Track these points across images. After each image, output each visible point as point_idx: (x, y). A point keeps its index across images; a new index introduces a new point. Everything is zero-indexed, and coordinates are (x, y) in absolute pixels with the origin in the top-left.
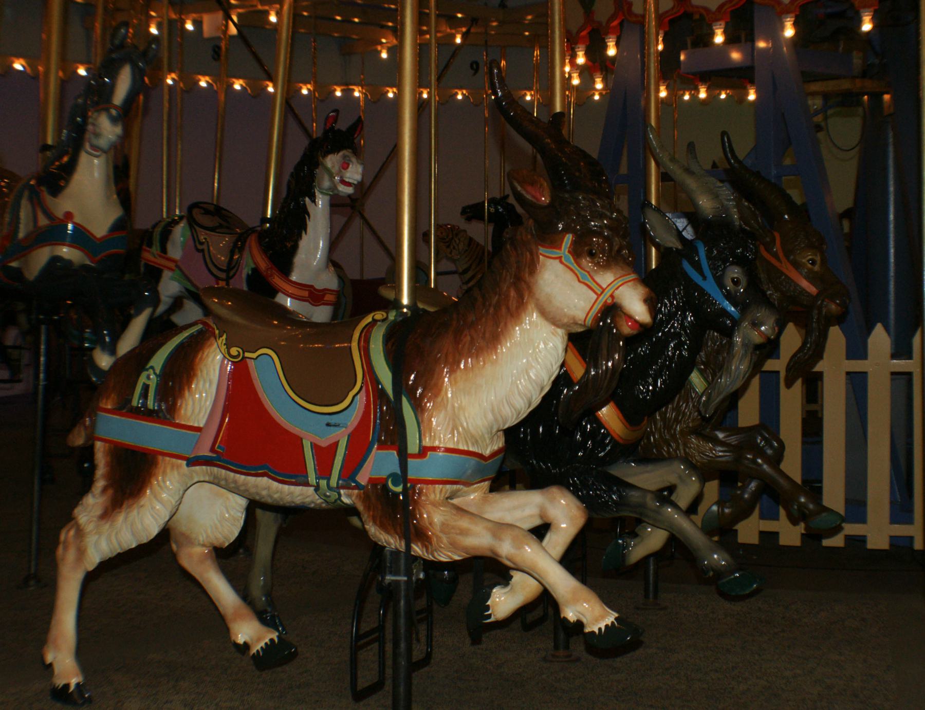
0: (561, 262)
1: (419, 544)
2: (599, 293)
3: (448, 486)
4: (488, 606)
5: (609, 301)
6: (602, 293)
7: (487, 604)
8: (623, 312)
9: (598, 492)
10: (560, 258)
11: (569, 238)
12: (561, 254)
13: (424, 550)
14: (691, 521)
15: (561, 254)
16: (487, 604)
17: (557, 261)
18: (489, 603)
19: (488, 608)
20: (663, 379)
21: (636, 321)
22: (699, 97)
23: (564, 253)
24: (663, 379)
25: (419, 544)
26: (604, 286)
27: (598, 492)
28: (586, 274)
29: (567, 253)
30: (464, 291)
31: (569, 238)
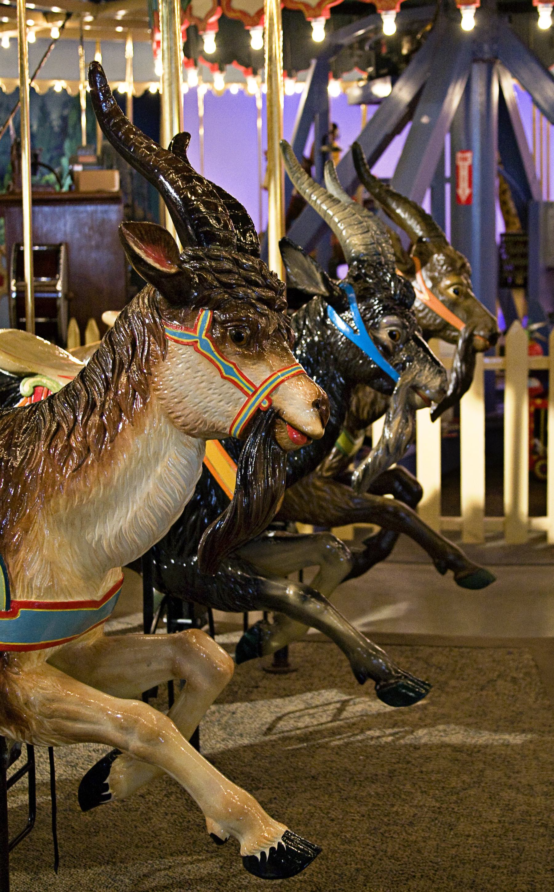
0: (197, 351)
1: (12, 728)
2: (250, 393)
3: (47, 650)
4: (107, 784)
5: (265, 405)
6: (254, 393)
7: (105, 782)
8: (284, 421)
9: (206, 521)
10: (194, 344)
11: (206, 315)
12: (194, 337)
13: (20, 735)
14: (391, 562)
15: (194, 337)
16: (105, 782)
17: (191, 349)
18: (107, 781)
19: (106, 787)
20: (336, 384)
21: (303, 434)
22: (385, 36)
23: (200, 338)
24: (336, 384)
25: (12, 728)
26: (258, 386)
27: (206, 521)
28: (231, 366)
29: (203, 337)
30: (253, 703)
31: (206, 315)
